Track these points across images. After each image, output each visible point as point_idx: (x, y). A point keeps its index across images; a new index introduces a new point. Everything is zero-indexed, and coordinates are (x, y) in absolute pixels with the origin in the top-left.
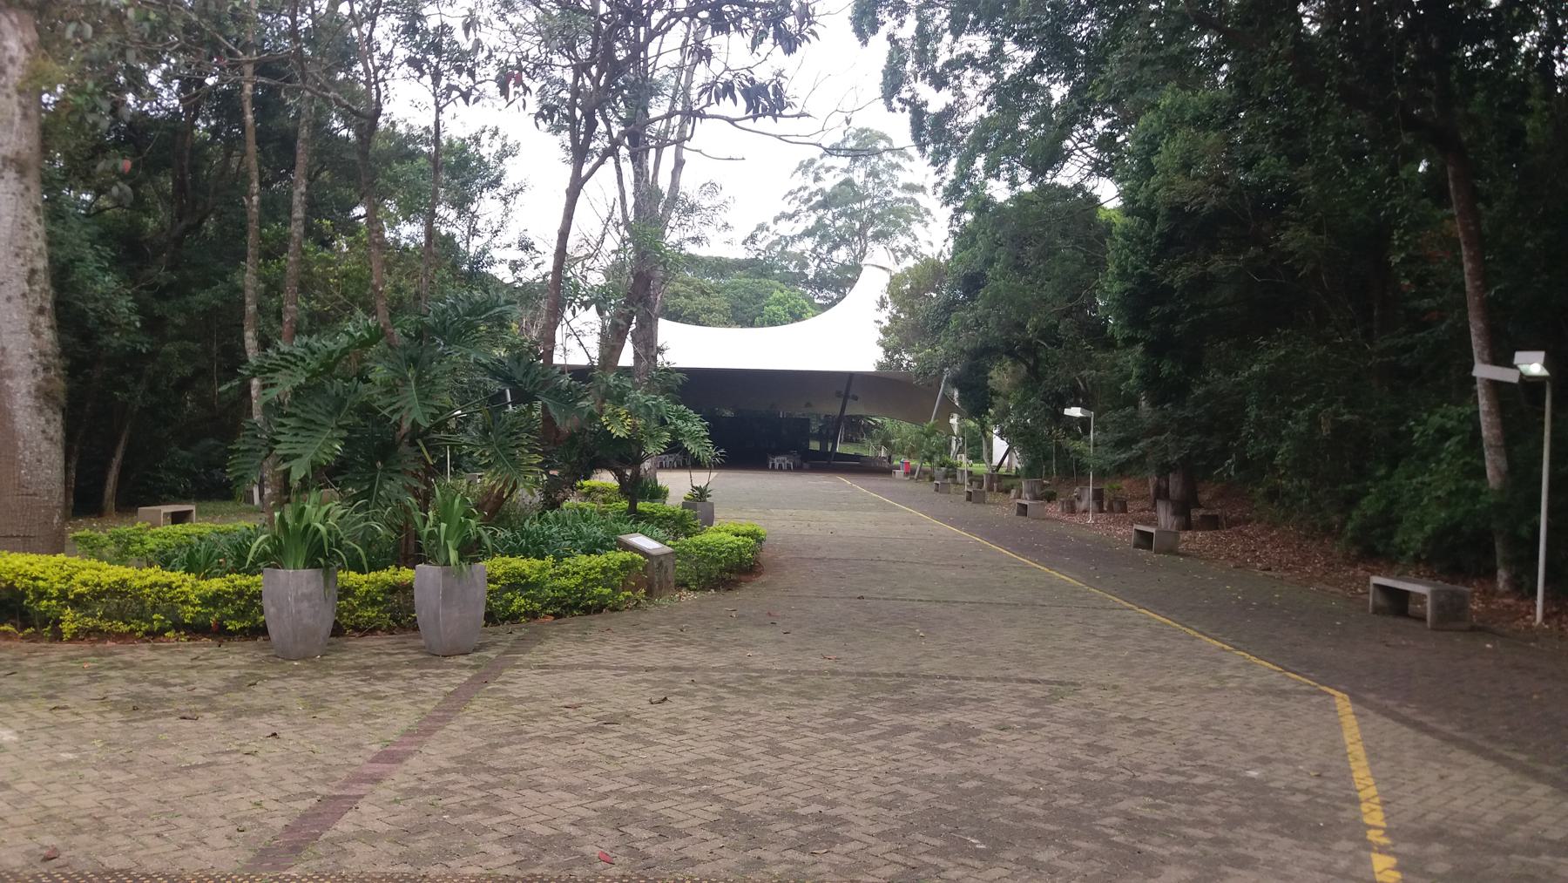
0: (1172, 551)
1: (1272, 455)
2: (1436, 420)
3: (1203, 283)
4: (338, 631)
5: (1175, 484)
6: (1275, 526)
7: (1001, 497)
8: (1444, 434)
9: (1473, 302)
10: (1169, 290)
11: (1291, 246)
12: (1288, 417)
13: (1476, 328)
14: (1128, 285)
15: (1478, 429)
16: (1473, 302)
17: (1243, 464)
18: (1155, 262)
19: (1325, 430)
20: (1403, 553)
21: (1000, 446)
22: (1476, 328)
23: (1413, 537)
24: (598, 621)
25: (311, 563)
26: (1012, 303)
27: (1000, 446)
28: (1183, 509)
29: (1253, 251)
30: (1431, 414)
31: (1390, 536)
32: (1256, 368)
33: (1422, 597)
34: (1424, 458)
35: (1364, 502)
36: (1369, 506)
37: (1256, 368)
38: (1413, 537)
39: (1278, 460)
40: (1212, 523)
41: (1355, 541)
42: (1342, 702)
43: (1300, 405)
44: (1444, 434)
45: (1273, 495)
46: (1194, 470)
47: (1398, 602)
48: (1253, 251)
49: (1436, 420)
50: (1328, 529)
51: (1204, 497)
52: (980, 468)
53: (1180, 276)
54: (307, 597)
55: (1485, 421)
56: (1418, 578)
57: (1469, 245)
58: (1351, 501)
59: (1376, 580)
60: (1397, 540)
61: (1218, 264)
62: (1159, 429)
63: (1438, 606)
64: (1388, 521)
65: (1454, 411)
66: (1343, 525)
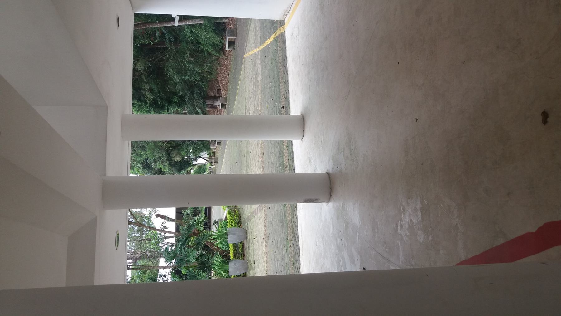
0: (226, 99)
1: (199, 73)
2: (188, 34)
3: (151, 90)
4: (244, 259)
5: (209, 102)
6: (218, 73)
7: (216, 155)
8: (191, 32)
9: (159, 25)
10: (153, 99)
11: (143, 68)
12: (188, 69)
13: (166, 25)
14: (152, 110)
15: (190, 25)
16: (159, 25)
17: (201, 80)
18: (146, 103)
19: (192, 59)
20: (221, 42)
21: (200, 161)
22: (166, 25)
23: (217, 40)
24: (242, 212)
25: (228, 263)
26: (154, 149)
27: (200, 161)
28: (215, 98)
29: (144, 77)
30: (187, 35)
31: (217, 45)
32: (176, 77)
33: (229, 39)
34: (198, 36)
35: (209, 51)
36: (210, 50)
37: (176, 77)
38: (217, 40)
39: (200, 71)
40: (219, 91)
41: (219, 53)
42: (245, 56)
43: (185, 66)
44: (191, 32)
45: (210, 73)
46: (205, 97)
47: (231, 44)
48: (144, 77)
49: (188, 34)
50: (217, 59)
51: (213, 94)
52: (208, 165)
53: (150, 96)
54: (235, 264)
55: (188, 23)
56: (225, 41)
57: (146, 26)
58: (209, 54)
59: (227, 49)
60: (218, 43)
61: (146, 86)
62: (193, 106)
63: (231, 35)
64: (214, 45)
65: (186, 30)
66: (215, 56)
